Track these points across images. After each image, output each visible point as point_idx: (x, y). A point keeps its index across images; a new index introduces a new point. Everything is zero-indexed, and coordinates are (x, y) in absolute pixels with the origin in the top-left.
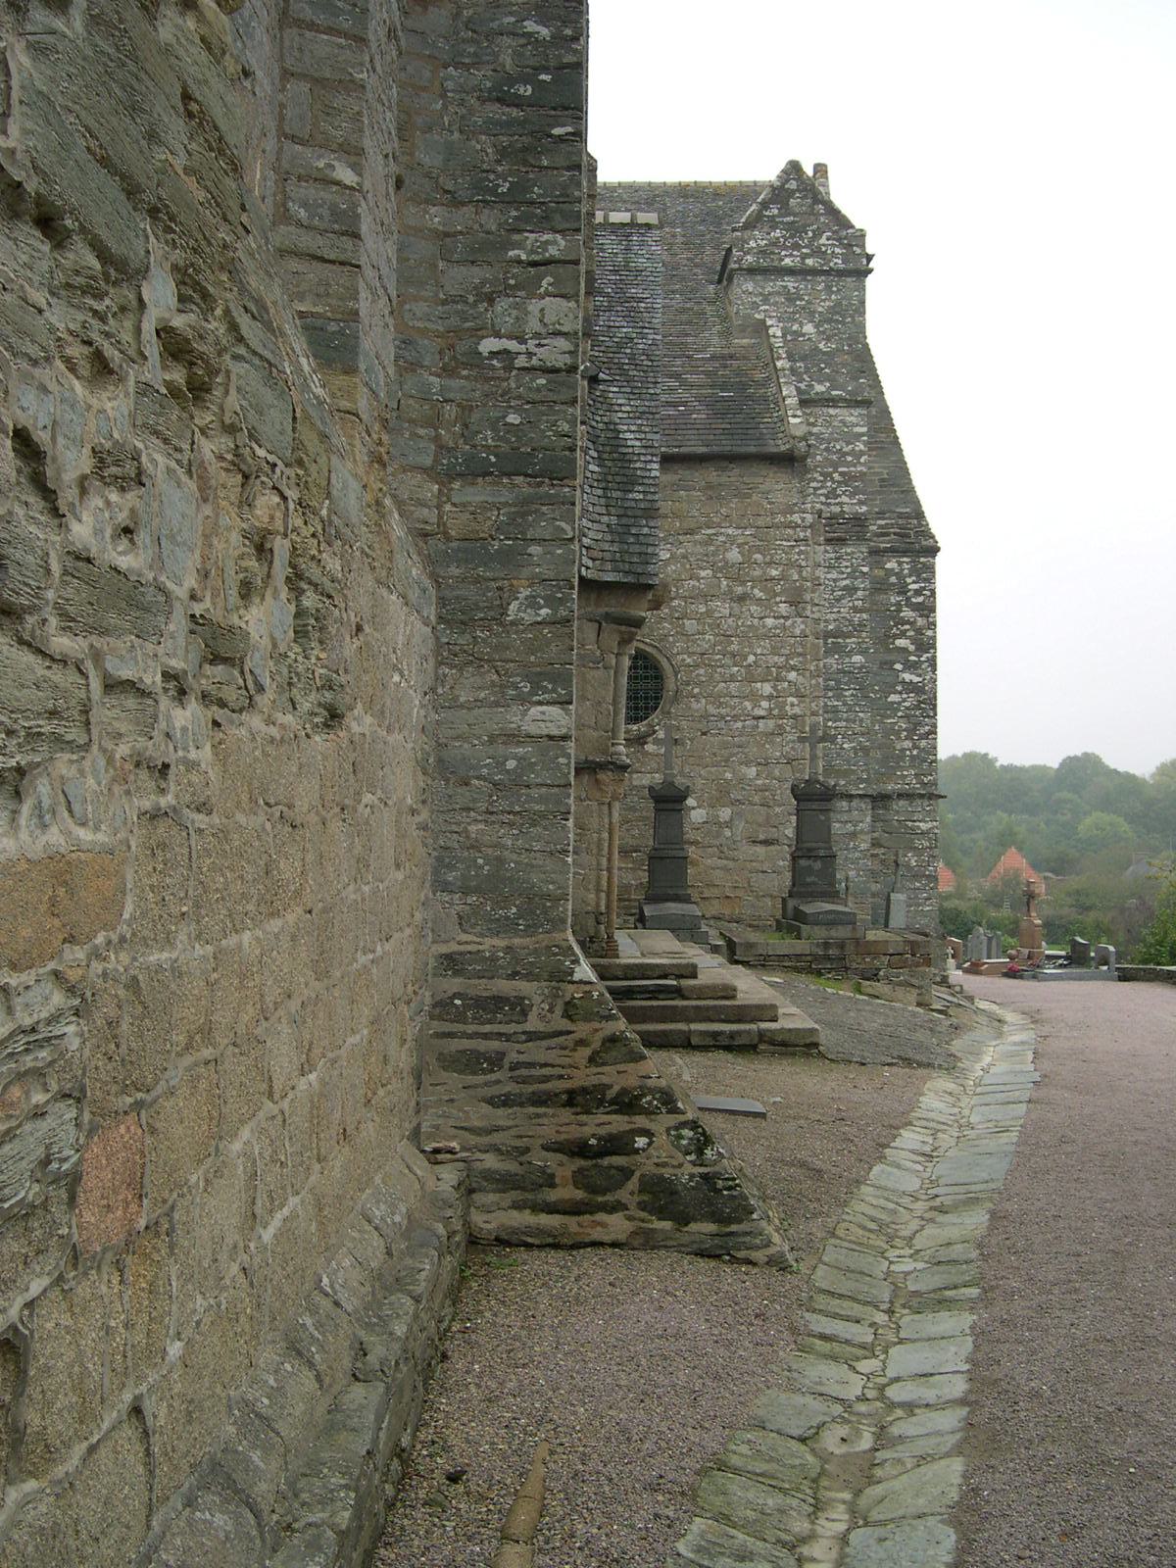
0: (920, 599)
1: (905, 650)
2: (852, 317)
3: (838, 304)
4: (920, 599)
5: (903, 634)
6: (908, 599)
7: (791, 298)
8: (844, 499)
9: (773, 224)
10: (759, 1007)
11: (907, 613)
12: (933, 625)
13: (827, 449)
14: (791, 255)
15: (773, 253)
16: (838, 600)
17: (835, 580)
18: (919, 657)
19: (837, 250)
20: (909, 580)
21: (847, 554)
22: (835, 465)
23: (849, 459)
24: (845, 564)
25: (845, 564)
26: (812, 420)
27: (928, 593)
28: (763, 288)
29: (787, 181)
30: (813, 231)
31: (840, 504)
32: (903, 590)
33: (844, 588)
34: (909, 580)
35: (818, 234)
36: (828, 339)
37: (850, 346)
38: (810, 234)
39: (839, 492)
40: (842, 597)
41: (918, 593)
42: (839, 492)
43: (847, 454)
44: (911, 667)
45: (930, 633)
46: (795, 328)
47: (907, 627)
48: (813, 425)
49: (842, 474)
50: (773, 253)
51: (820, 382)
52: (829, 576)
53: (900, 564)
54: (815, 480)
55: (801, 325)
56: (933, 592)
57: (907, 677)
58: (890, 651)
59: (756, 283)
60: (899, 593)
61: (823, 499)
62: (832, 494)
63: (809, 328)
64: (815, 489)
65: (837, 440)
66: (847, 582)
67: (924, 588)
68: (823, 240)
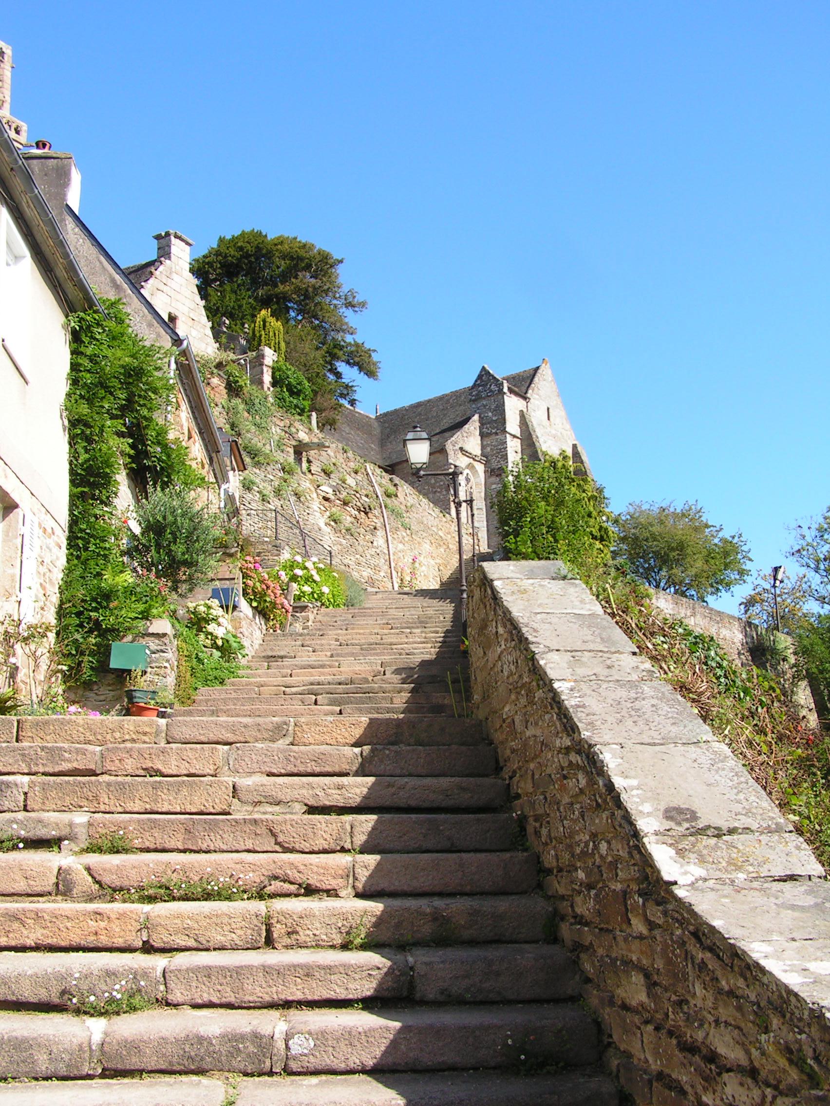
7: (485, 406)
9: (479, 386)
63: (490, 414)
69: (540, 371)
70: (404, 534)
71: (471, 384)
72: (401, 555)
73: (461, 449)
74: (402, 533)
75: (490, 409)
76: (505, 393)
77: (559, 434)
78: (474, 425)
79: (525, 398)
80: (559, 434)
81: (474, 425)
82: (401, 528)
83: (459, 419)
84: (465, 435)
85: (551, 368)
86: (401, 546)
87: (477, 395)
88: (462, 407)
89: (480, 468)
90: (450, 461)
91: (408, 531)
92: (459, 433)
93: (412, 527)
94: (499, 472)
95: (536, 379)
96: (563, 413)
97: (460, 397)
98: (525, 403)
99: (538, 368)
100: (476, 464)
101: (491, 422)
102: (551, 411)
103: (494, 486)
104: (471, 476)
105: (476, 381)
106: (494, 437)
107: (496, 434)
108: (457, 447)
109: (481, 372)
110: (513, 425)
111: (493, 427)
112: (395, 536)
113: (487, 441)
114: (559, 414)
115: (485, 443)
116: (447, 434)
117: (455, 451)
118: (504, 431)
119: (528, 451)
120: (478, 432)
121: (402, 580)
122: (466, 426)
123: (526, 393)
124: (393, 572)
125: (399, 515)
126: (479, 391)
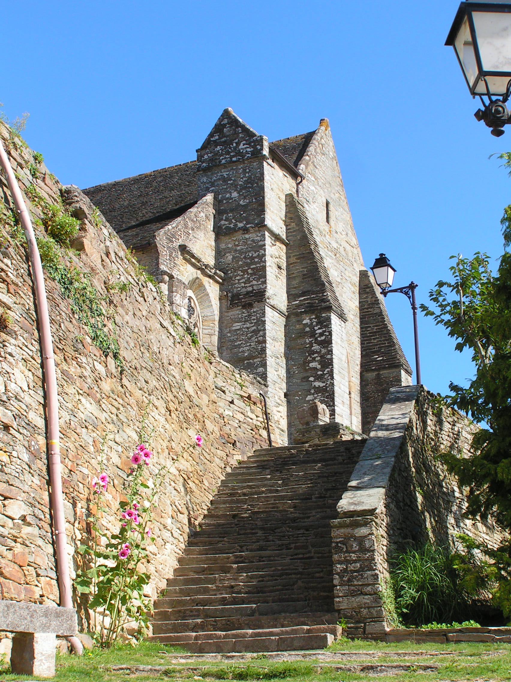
0: (323, 338)
1: (315, 369)
2: (257, 183)
3: (250, 177)
4: (323, 338)
5: (314, 360)
6: (316, 339)
7: (225, 180)
8: (255, 282)
9: (216, 143)
10: (424, 641)
11: (316, 347)
12: (330, 352)
13: (245, 258)
14: (225, 158)
15: (217, 159)
16: (250, 339)
17: (248, 328)
18: (323, 371)
19: (248, 150)
20: (316, 328)
21: (254, 312)
22: (248, 265)
23: (256, 260)
24: (253, 318)
25: (253, 318)
26: (237, 243)
27: (327, 334)
28: (211, 179)
29: (222, 120)
30: (236, 143)
31: (252, 286)
32: (313, 334)
33: (253, 331)
34: (316, 328)
35: (238, 144)
36: (245, 198)
37: (256, 199)
38: (235, 145)
39: (251, 279)
40: (252, 336)
41: (321, 335)
42: (251, 279)
43: (256, 257)
44: (319, 378)
45: (329, 357)
46: (227, 196)
47: (316, 355)
48: (238, 246)
49: (252, 269)
50: (217, 159)
51: (241, 222)
52: (245, 326)
53: (311, 320)
54: (238, 275)
55: (231, 193)
56: (330, 334)
57: (317, 384)
58: (306, 371)
59: (208, 177)
60: (311, 337)
61: (243, 285)
62: (248, 281)
63: (235, 194)
64: (238, 280)
65: (250, 251)
66: (255, 328)
67: (325, 331)
68: (241, 146)
69: (317, 137)
70: (100, 368)
71: (200, 148)
72: (87, 437)
73: (183, 249)
74: (93, 363)
75: (235, 186)
76: (264, 157)
77: (342, 249)
78: (204, 211)
79: (295, 175)
80: (342, 249)
81: (204, 211)
82: (94, 350)
83: (170, 208)
84: (190, 224)
85: (334, 137)
86: (88, 407)
87: (211, 160)
88: (175, 193)
89: (213, 290)
90: (163, 267)
91: (111, 361)
92: (179, 219)
93: (123, 353)
94: (248, 300)
95: (311, 149)
96: (347, 216)
97: (171, 177)
98: (293, 183)
99: (308, 138)
100: (206, 281)
101: (237, 208)
102: (331, 207)
103: (237, 326)
104: (195, 303)
105: (211, 135)
106: (239, 236)
107: (246, 230)
108: (176, 244)
109: (221, 119)
110: (275, 218)
111: (241, 216)
112: (73, 370)
113: (228, 243)
114: (341, 215)
115: (223, 246)
116: (153, 226)
117: (171, 250)
118: (261, 225)
119: (299, 269)
120: (210, 225)
121: (88, 529)
122: (193, 210)
123: (296, 164)
124: (60, 498)
125: (85, 304)
126: (217, 154)
